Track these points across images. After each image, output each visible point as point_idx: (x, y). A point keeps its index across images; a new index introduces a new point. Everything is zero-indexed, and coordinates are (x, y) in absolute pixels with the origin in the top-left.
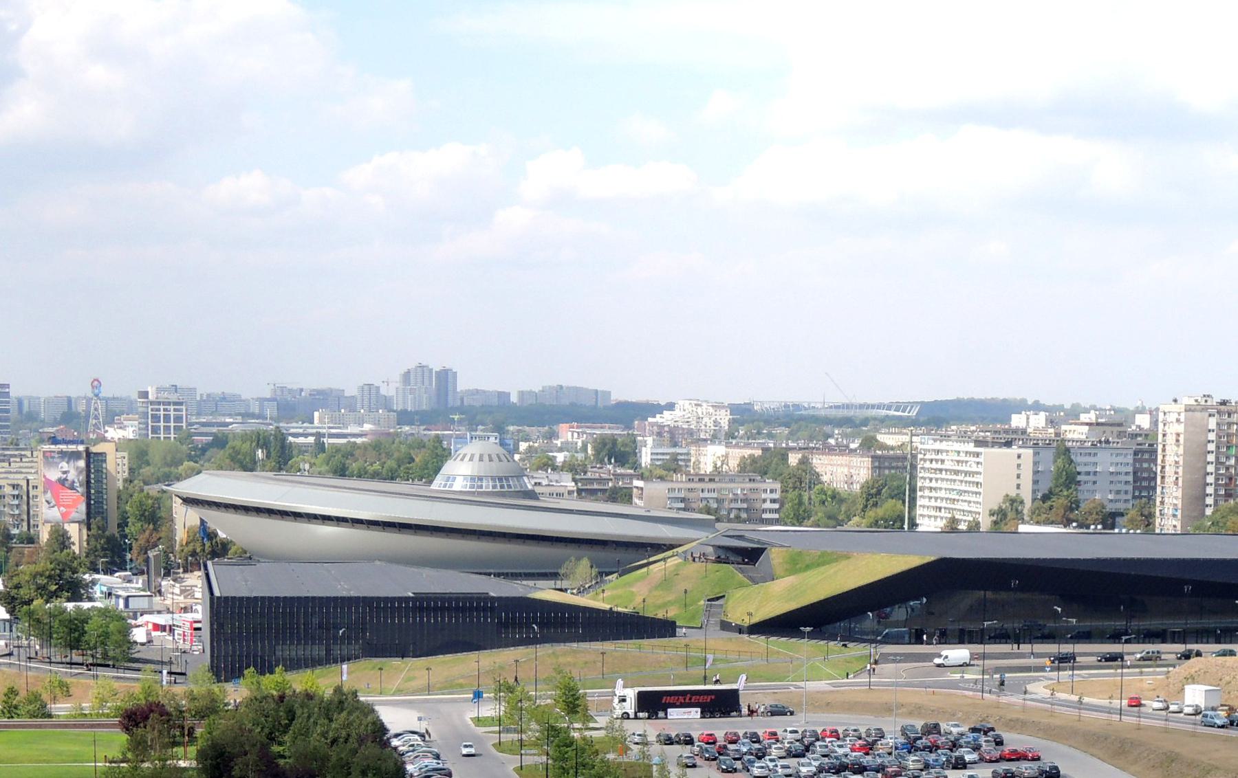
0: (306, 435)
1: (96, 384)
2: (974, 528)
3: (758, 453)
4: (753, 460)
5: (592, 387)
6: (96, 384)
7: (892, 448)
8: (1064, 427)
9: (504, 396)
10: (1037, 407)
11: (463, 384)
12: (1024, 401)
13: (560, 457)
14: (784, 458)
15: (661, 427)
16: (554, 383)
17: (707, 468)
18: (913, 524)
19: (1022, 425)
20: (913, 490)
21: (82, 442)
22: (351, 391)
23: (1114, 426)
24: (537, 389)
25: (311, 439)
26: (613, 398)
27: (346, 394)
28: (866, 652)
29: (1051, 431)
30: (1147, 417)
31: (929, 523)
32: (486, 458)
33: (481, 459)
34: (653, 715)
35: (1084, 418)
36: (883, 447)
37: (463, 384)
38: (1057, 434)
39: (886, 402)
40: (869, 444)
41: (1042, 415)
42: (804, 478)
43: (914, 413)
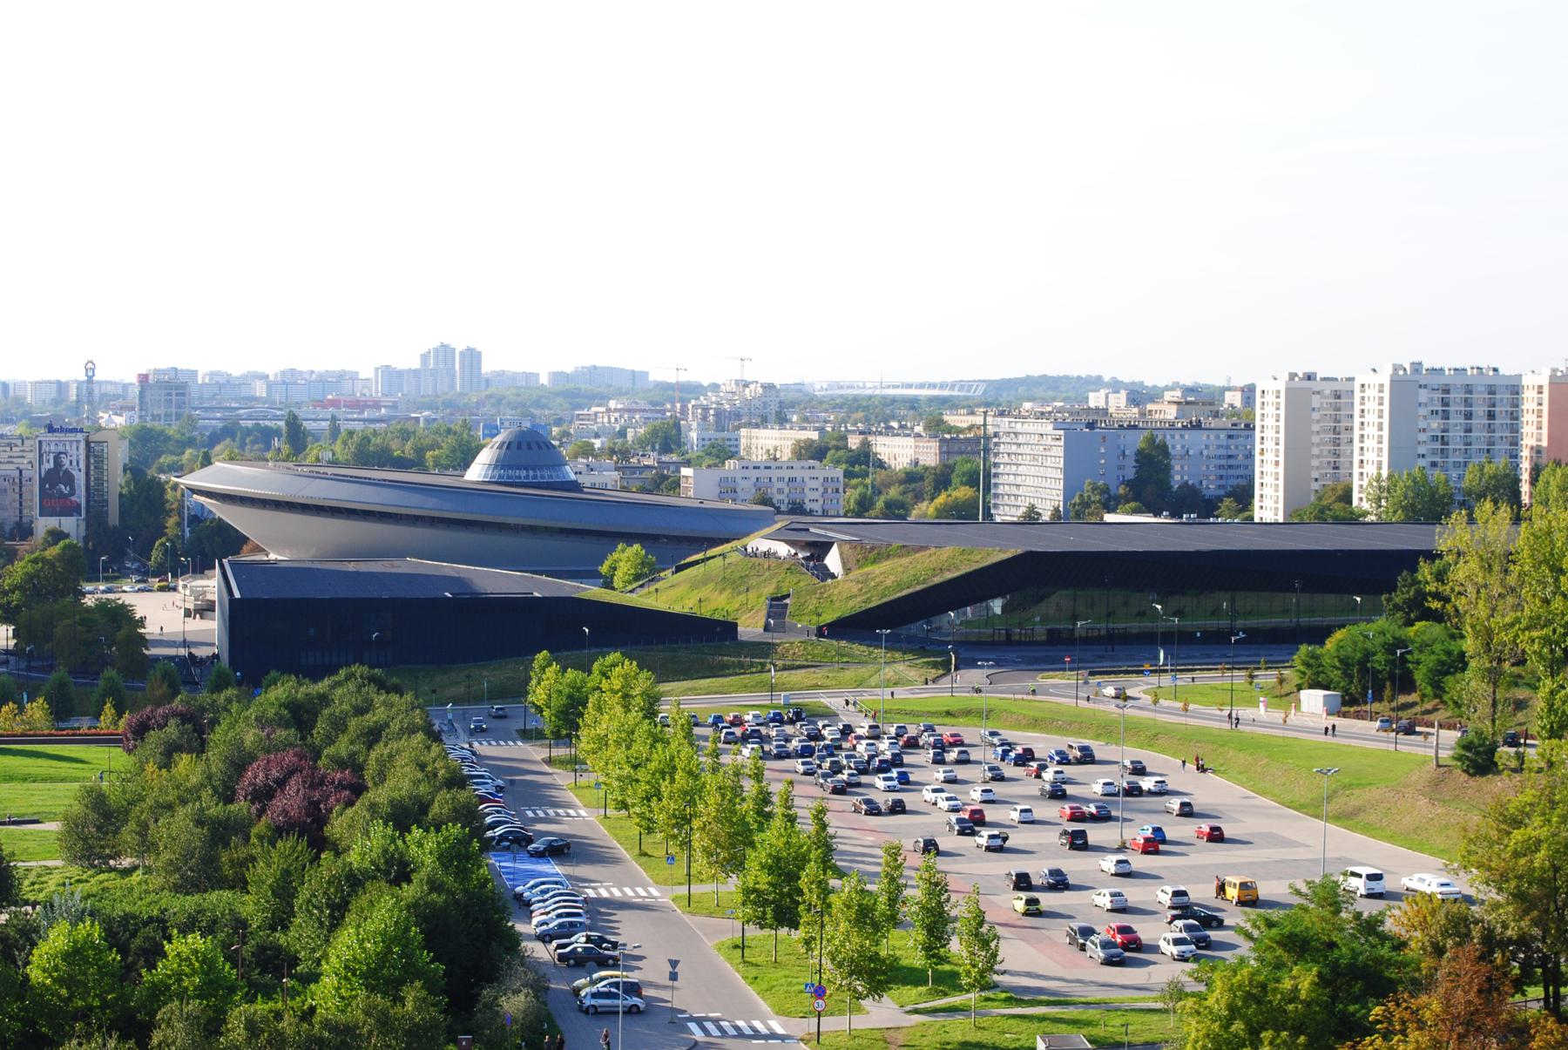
0: (276, 418)
1: (90, 368)
2: (1031, 518)
3: (815, 436)
4: (810, 442)
5: (629, 366)
6: (90, 368)
7: (960, 431)
8: (1150, 407)
9: (531, 377)
10: (1115, 386)
11: (488, 366)
12: (1099, 378)
13: (597, 443)
14: (844, 438)
15: (706, 409)
16: (588, 364)
17: (759, 456)
18: (988, 515)
19: (1102, 405)
20: (988, 476)
21: (81, 431)
22: (705, 384)
23: (1200, 403)
24: (569, 369)
25: (325, 424)
26: (651, 378)
27: (361, 376)
28: (1226, 683)
29: (1136, 410)
30: (1238, 395)
31: (1006, 513)
32: (524, 446)
33: (519, 447)
34: (1023, 765)
35: (1168, 396)
36: (950, 430)
37: (488, 366)
38: (1142, 414)
39: (949, 380)
40: (936, 426)
41: (1123, 394)
42: (863, 460)
43: (979, 392)
